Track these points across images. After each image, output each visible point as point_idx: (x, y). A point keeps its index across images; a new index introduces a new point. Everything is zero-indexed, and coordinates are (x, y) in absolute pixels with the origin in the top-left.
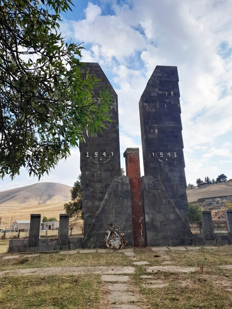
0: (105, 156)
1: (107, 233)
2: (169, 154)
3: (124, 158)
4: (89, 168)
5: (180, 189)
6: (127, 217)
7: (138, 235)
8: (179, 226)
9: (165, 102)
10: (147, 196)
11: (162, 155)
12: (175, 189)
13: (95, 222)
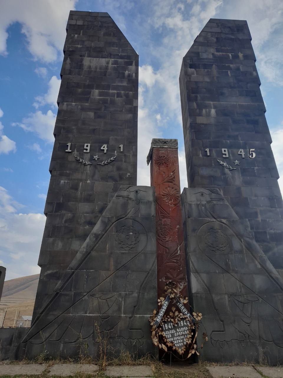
0: (105, 151)
1: (159, 304)
2: (242, 152)
3: (148, 164)
4: (68, 172)
5: (270, 221)
6: (144, 280)
9: (229, 68)
10: (194, 230)
11: (227, 153)
12: (260, 221)
13: (62, 287)
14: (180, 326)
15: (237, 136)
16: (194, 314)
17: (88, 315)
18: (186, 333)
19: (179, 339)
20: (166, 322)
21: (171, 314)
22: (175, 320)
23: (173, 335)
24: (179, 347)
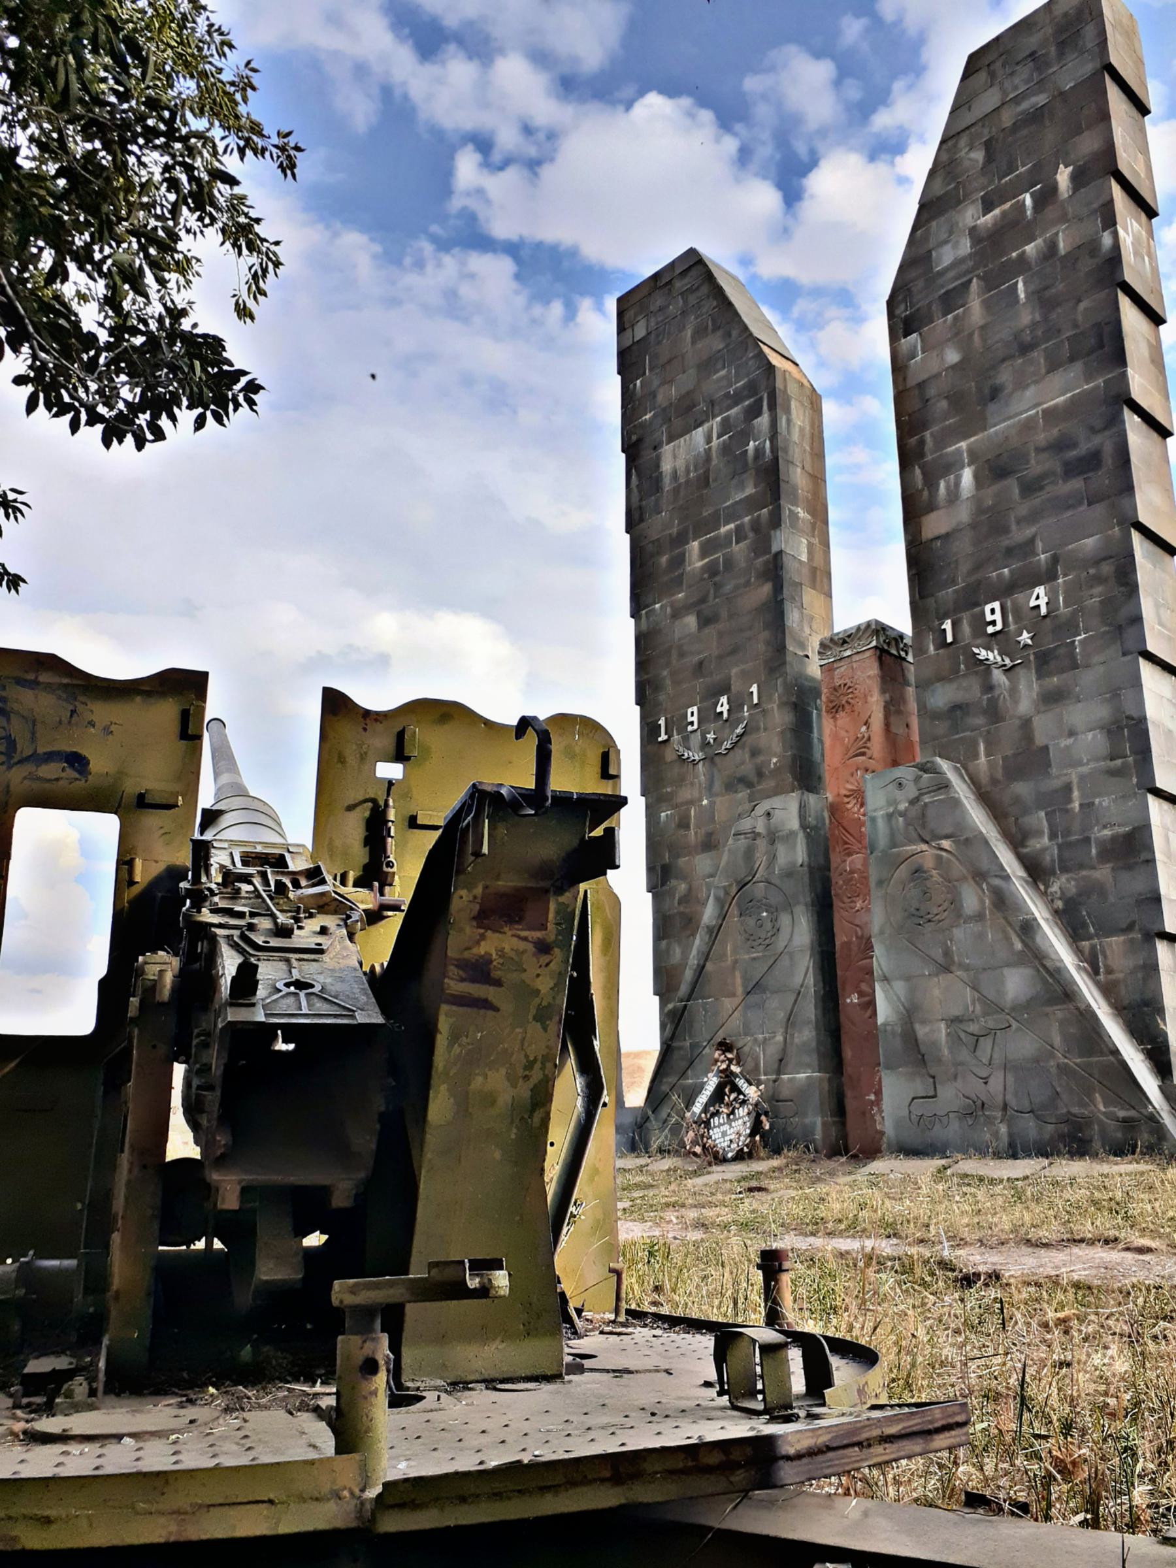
0: (725, 715)
4: (669, 790)
7: (872, 1097)
8: (1057, 1040)
10: (880, 883)
11: (998, 617)
12: (1077, 809)
15: (1032, 541)
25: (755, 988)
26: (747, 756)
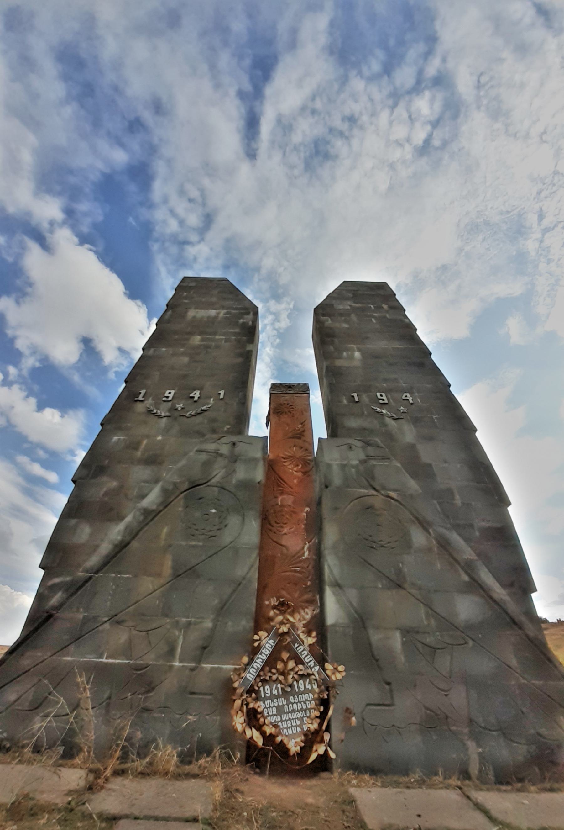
0: (196, 399)
1: (256, 644)
3: (267, 426)
14: (297, 691)
16: (328, 666)
17: (104, 660)
18: (309, 707)
19: (294, 717)
20: (267, 681)
21: (280, 666)
22: (286, 679)
23: (280, 710)
24: (293, 736)
25: (185, 573)
26: (206, 421)
